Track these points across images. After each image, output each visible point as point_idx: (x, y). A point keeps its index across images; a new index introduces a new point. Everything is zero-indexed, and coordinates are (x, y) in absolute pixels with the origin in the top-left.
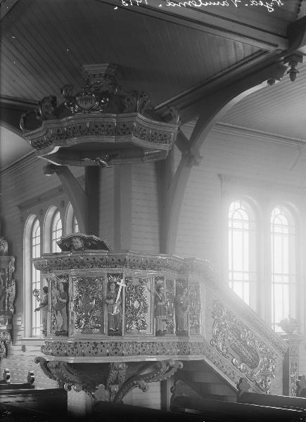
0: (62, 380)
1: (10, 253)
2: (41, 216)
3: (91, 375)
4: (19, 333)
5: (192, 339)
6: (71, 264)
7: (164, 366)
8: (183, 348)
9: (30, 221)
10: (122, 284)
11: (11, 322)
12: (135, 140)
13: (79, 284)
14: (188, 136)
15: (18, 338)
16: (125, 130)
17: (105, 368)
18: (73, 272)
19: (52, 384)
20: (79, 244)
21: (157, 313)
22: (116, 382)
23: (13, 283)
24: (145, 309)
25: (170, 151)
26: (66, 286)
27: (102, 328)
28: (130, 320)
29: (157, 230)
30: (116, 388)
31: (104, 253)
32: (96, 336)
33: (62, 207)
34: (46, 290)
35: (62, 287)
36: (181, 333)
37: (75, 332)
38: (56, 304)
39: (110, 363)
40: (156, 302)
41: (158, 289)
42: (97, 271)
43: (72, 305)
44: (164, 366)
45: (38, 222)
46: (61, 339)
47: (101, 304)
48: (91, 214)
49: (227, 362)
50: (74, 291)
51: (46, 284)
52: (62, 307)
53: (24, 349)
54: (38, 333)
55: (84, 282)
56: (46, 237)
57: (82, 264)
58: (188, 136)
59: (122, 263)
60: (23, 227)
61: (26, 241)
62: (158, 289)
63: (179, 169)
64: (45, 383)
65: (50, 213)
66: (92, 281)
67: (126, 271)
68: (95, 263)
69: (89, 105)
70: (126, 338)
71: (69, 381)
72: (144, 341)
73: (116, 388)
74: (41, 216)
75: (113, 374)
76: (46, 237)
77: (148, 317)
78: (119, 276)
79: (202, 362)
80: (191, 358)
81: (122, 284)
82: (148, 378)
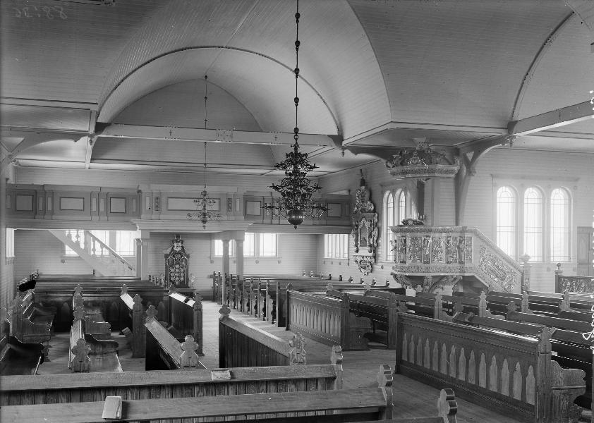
0: (403, 283)
1: (374, 211)
2: (393, 192)
3: (416, 280)
4: (380, 258)
5: (467, 265)
6: (407, 231)
7: (450, 277)
8: (462, 270)
9: (387, 194)
10: (430, 241)
11: (375, 252)
12: (436, 175)
13: (411, 240)
14: (470, 159)
15: (379, 261)
16: (432, 171)
17: (422, 278)
18: (408, 234)
19: (398, 286)
20: (411, 223)
21: (448, 252)
22: (427, 285)
23: (376, 228)
24: (442, 252)
25: (459, 171)
26: (405, 241)
27: (421, 260)
28: (434, 257)
29: (454, 201)
30: (427, 288)
31: (422, 227)
32: (418, 263)
33: (405, 190)
34: (396, 241)
35: (403, 241)
36: (461, 262)
37: (409, 262)
38: (401, 248)
39: (170, 331)
40: (447, 248)
41: (448, 242)
42: (419, 234)
43: (407, 249)
44: (450, 277)
45: (391, 195)
46: (403, 265)
47: (421, 249)
48: (420, 201)
49: (487, 277)
50: (409, 243)
51: (396, 238)
52: (404, 250)
53: (382, 268)
54: (391, 258)
55: (414, 239)
56: (396, 204)
57: (412, 231)
58: (470, 159)
59: (431, 231)
60: (383, 197)
61: (385, 205)
62: (448, 242)
63: (465, 177)
64: (395, 285)
65: (398, 192)
66: (416, 239)
67: (432, 235)
68: (418, 231)
69: (416, 162)
70: (431, 265)
71: (406, 284)
72: (439, 265)
73: (427, 288)
74: (393, 192)
75: (426, 281)
76: (396, 204)
77: (443, 255)
78: (428, 236)
79: (473, 276)
80: (466, 274)
81: (430, 241)
82: (444, 284)
